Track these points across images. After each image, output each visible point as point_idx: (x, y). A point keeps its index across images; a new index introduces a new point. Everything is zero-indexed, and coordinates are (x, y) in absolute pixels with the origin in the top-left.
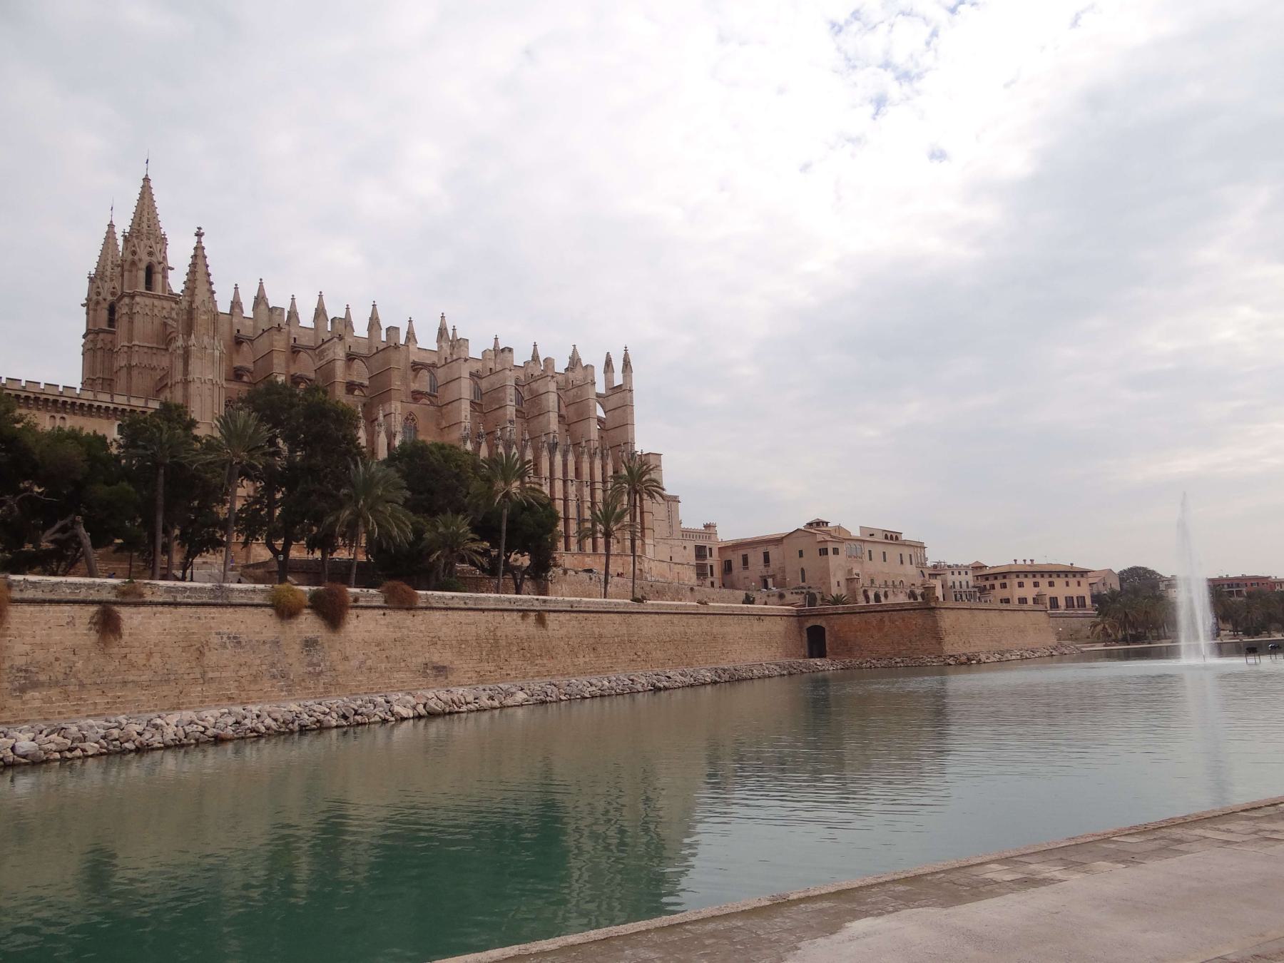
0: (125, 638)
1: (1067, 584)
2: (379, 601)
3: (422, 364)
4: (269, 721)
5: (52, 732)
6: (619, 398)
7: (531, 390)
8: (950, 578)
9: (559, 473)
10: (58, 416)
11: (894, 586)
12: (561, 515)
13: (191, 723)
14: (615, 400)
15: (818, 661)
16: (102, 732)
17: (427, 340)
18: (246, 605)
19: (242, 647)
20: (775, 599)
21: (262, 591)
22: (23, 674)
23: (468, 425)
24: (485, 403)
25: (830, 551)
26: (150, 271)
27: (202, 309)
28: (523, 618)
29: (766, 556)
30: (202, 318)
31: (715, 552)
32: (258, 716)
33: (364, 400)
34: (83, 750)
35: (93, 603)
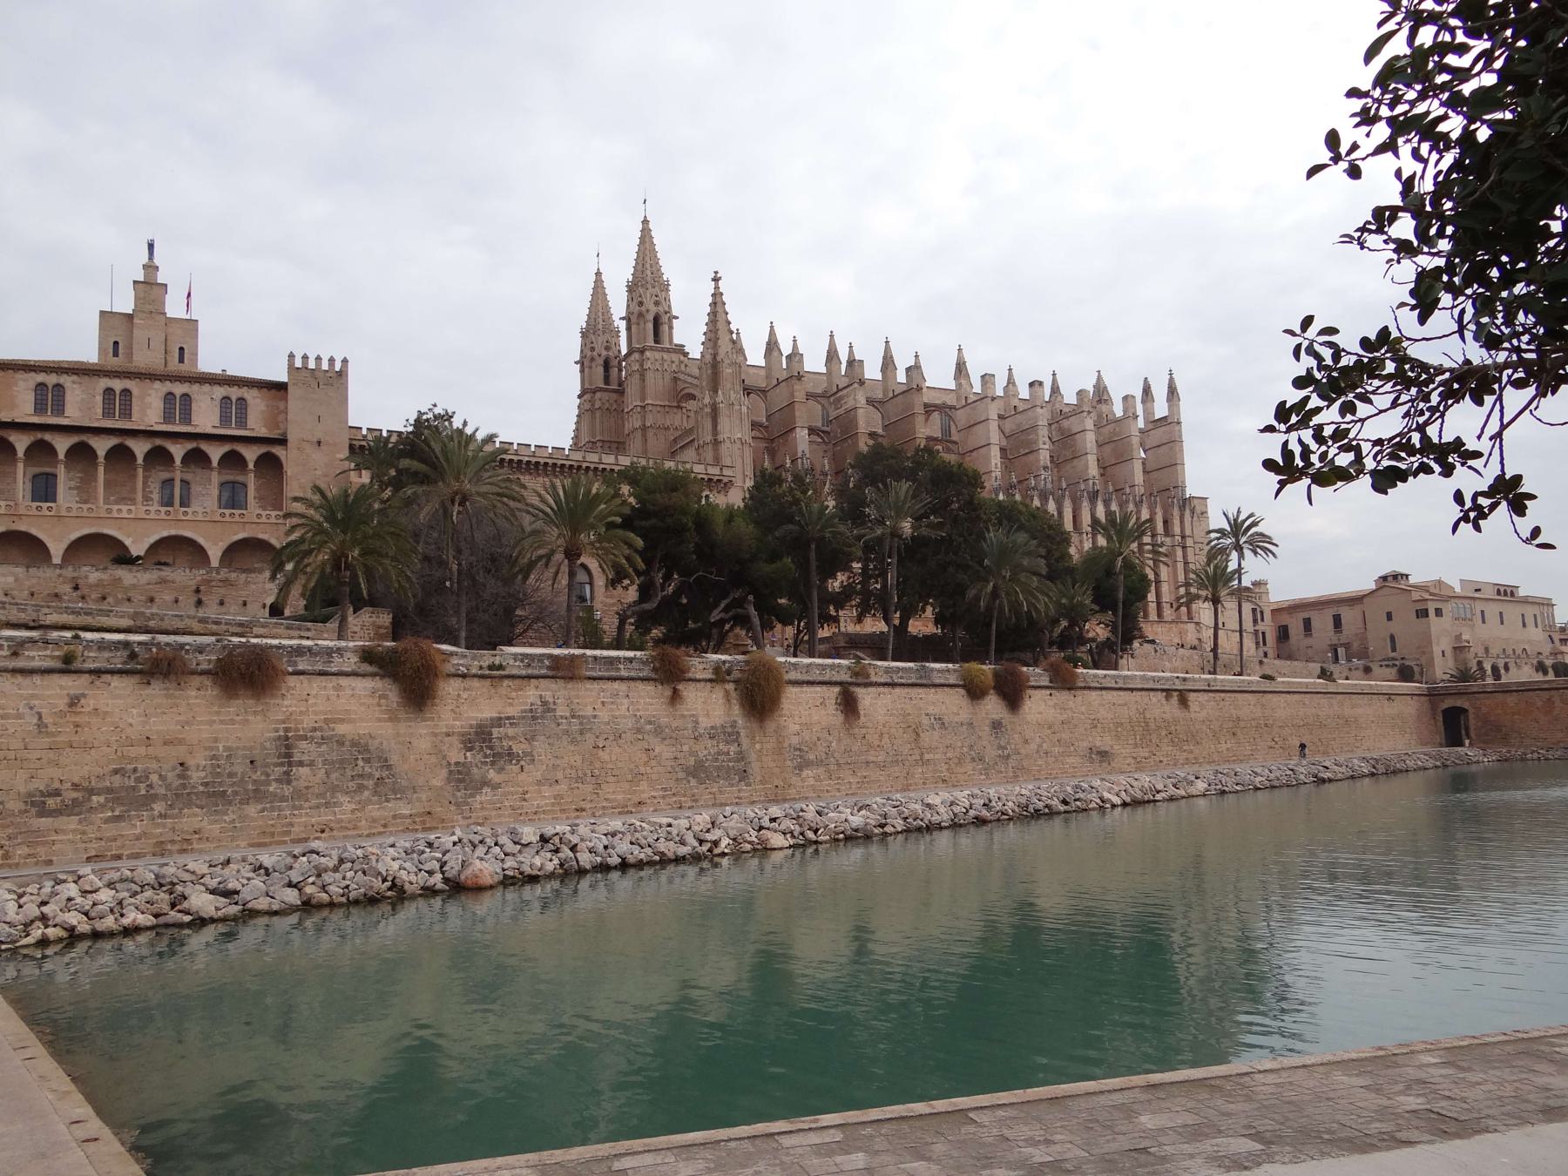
2: (1045, 681)
3: (935, 406)
14: (1158, 436)
17: (939, 377)
20: (1360, 673)
25: (1432, 613)
26: (657, 321)
27: (727, 361)
28: (1167, 698)
29: (1337, 621)
30: (727, 371)
31: (1267, 616)
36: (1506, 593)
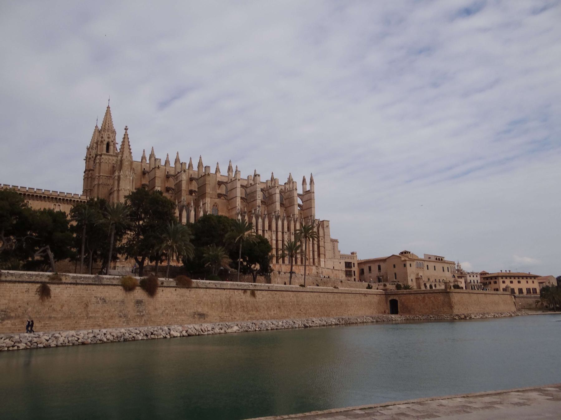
0: (52, 298)
1: (527, 282)
2: (174, 284)
4: (109, 336)
5: (7, 338)
6: (308, 196)
7: (269, 193)
8: (469, 279)
9: (280, 229)
10: (57, 204)
11: (439, 281)
12: (274, 246)
13: (73, 336)
14: (306, 197)
15: (393, 316)
16: (30, 339)
18: (109, 285)
19: (106, 303)
21: (117, 279)
22: (4, 313)
23: (240, 208)
24: (248, 199)
26: (108, 145)
27: (126, 160)
29: (379, 267)
30: (126, 163)
31: (356, 265)
32: (105, 334)
33: (195, 198)
34: (18, 347)
35: (38, 283)
36: (439, 259)
